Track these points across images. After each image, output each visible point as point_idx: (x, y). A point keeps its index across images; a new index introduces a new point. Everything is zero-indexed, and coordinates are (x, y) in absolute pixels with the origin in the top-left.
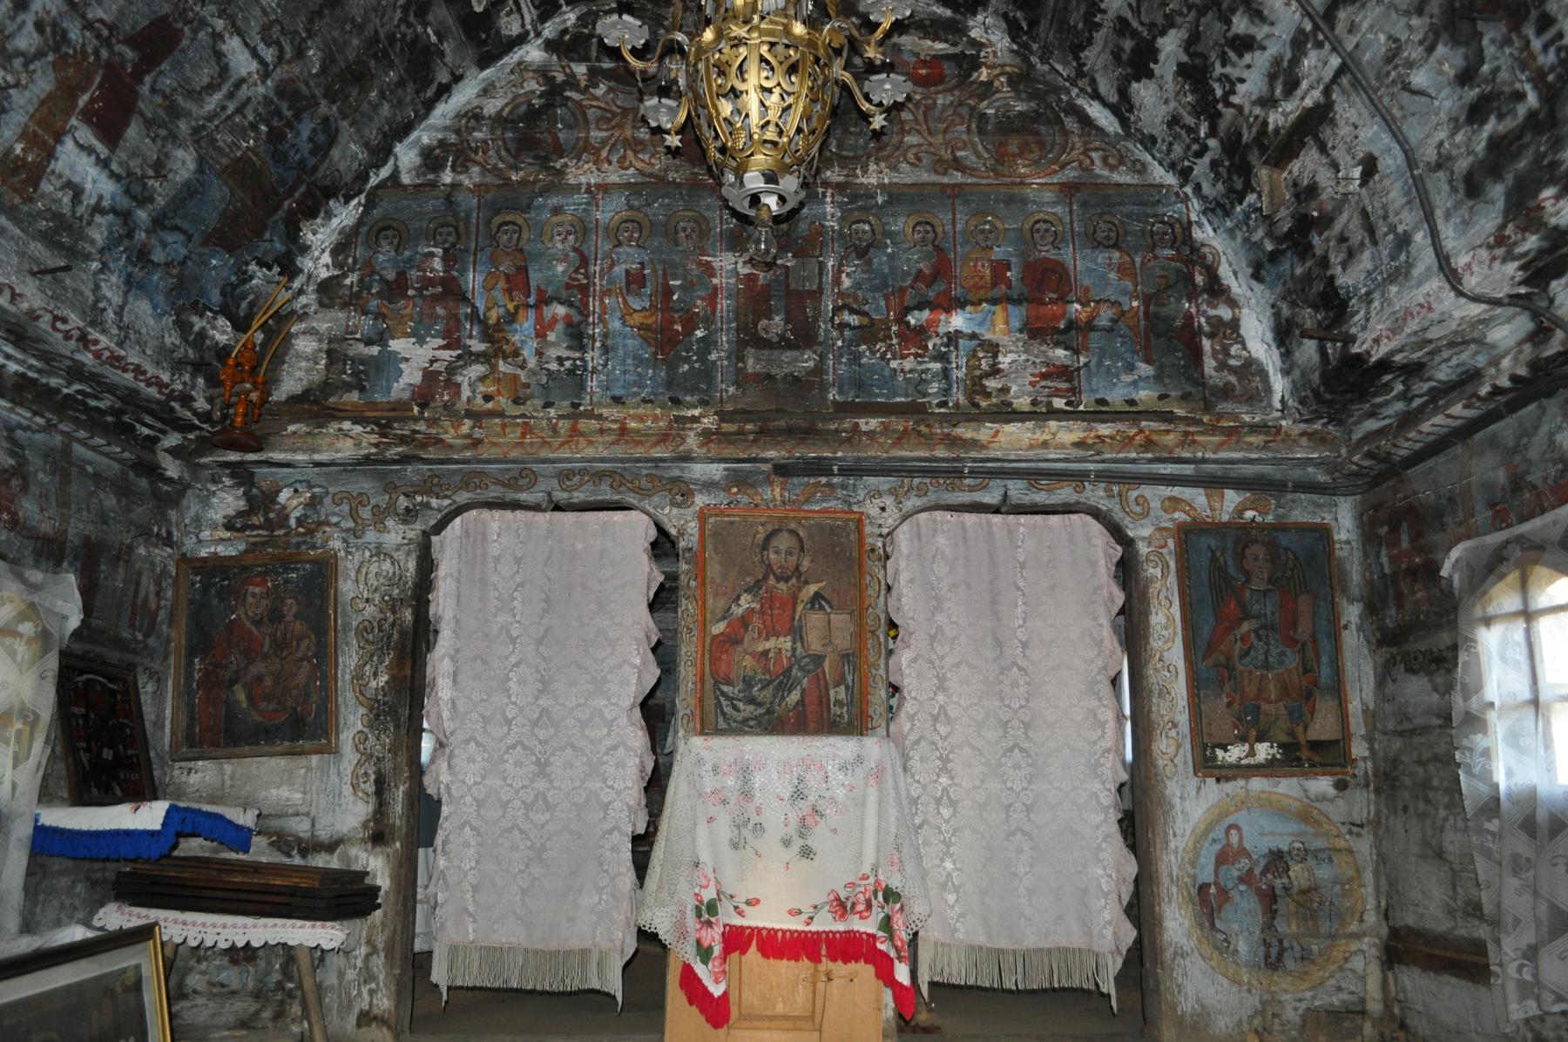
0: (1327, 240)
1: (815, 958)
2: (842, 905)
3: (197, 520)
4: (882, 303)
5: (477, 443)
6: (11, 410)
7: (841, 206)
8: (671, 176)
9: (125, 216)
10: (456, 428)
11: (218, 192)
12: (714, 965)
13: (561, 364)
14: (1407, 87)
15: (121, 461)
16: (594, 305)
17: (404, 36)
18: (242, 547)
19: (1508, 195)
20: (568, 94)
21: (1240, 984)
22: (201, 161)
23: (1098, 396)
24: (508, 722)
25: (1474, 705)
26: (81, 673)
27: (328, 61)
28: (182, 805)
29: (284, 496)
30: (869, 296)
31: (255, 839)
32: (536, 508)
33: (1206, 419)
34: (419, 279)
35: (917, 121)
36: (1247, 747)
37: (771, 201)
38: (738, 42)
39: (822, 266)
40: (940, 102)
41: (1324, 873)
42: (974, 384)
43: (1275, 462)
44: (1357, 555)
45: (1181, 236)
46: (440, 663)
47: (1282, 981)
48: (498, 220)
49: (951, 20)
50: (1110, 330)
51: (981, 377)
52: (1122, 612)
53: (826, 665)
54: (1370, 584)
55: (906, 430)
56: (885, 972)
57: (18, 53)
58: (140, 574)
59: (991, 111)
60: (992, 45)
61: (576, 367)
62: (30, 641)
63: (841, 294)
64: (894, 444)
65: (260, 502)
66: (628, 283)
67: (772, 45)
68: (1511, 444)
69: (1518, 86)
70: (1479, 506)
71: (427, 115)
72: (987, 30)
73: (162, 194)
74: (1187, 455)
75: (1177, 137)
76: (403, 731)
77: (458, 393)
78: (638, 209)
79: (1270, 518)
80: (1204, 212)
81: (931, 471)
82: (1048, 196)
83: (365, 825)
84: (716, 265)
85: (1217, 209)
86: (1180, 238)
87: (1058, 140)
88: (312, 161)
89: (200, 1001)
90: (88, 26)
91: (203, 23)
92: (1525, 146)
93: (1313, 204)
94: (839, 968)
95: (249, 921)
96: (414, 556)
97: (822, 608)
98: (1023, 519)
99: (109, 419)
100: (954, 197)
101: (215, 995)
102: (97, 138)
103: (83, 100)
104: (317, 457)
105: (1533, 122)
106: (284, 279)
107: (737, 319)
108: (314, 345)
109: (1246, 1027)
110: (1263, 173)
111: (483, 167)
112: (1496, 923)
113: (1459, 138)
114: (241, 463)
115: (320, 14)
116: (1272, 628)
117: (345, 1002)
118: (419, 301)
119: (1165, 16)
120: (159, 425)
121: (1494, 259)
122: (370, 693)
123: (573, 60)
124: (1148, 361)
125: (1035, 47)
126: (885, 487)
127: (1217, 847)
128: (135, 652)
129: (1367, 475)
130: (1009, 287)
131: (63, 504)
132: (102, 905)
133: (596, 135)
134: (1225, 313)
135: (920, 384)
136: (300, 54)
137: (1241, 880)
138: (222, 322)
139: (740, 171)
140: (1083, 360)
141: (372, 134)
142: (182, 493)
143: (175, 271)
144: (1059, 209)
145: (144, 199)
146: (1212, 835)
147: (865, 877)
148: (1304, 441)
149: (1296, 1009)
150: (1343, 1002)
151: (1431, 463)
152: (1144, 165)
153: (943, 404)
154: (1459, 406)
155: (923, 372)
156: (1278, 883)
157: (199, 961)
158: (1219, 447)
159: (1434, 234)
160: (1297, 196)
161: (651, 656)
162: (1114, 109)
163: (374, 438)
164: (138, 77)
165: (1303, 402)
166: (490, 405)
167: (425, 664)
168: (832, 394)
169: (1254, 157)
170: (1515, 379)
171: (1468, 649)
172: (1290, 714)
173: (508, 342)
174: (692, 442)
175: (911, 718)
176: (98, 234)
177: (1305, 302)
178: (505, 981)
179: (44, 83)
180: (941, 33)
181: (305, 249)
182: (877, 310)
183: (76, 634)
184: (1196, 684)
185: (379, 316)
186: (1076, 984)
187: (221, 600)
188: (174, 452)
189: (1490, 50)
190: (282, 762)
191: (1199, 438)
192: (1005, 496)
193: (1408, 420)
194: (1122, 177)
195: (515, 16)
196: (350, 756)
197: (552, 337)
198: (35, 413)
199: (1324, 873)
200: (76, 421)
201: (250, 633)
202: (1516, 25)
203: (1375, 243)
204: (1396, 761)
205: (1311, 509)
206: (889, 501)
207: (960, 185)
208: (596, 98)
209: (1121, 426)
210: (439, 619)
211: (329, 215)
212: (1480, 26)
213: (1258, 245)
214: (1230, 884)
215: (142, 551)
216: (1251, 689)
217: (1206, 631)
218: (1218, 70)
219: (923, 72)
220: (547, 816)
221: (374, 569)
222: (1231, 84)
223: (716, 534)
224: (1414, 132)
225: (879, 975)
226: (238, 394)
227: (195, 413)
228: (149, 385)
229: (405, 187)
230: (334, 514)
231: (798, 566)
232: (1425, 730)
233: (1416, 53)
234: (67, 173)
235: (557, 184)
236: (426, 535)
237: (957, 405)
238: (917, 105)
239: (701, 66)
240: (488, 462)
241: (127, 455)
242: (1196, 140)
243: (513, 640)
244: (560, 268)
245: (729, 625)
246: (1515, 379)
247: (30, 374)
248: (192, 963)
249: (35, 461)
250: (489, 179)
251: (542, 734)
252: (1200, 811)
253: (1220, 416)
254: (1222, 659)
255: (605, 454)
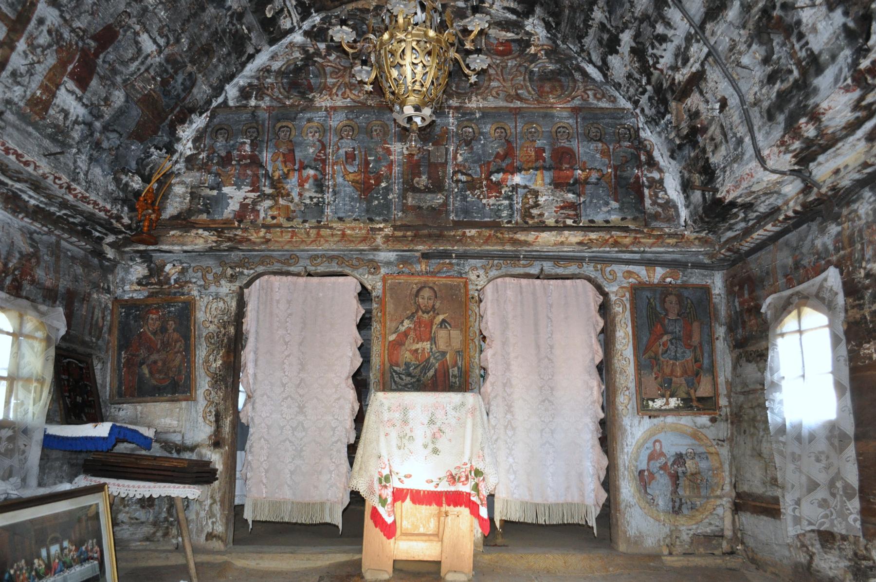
0: (705, 139)
1: (439, 504)
2: (453, 477)
3: (123, 280)
4: (478, 169)
5: (268, 241)
6: (31, 224)
7: (457, 118)
8: (369, 102)
9: (89, 125)
10: (257, 233)
11: (136, 112)
12: (388, 507)
13: (312, 200)
14: (739, 64)
15: (85, 250)
16: (329, 170)
17: (231, 30)
18: (146, 294)
19: (786, 120)
20: (315, 59)
21: (659, 521)
22: (127, 97)
23: (590, 218)
24: (284, 385)
25: (776, 377)
26: (65, 358)
27: (192, 43)
28: (118, 424)
29: (168, 268)
30: (472, 165)
31: (154, 444)
32: (298, 275)
33: (645, 230)
34: (239, 156)
35: (497, 74)
36: (665, 400)
37: (418, 120)
38: (400, 41)
39: (447, 150)
40: (509, 64)
41: (703, 465)
42: (526, 212)
43: (681, 253)
44: (724, 301)
45: (634, 135)
46: (248, 355)
47: (681, 520)
48: (279, 125)
49: (516, 21)
50: (596, 184)
51: (529, 208)
52: (603, 331)
53: (448, 356)
54: (730, 316)
55: (490, 235)
56: (474, 509)
57: (39, 46)
58: (94, 308)
59: (536, 69)
60: (537, 34)
61: (319, 202)
62: (41, 340)
63: (457, 165)
64: (484, 242)
65: (155, 271)
66: (347, 158)
67: (418, 42)
68: (795, 245)
69: (789, 66)
70: (780, 276)
71: (242, 70)
72: (535, 26)
73: (108, 113)
74: (636, 249)
75: (631, 84)
76: (229, 389)
77: (258, 215)
78: (352, 120)
79: (679, 282)
80: (646, 123)
81: (503, 257)
82: (565, 114)
83: (210, 438)
84: (392, 149)
85: (653, 121)
86: (633, 136)
87: (571, 84)
88: (183, 95)
89: (125, 527)
90: (73, 30)
91: (130, 27)
92: (793, 97)
93: (698, 121)
94: (452, 509)
95: (152, 484)
96: (235, 299)
97: (446, 327)
98: (552, 282)
99: (79, 228)
100: (516, 114)
101: (133, 524)
102: (76, 86)
103: (70, 67)
104: (185, 248)
105: (796, 85)
106: (168, 156)
107: (403, 177)
108: (184, 190)
109: (662, 543)
110: (673, 104)
111: (271, 97)
112: (783, 488)
113: (764, 91)
114: (145, 251)
115: (188, 21)
116: (678, 339)
117: (200, 528)
118: (238, 167)
119: (624, 23)
120: (104, 231)
121: (780, 152)
122: (212, 370)
123: (318, 41)
124: (616, 200)
125: (559, 36)
126: (479, 265)
127: (649, 451)
128: (91, 348)
129: (729, 260)
130: (544, 161)
131: (57, 271)
132: (76, 476)
133: (330, 81)
134: (656, 175)
135: (497, 211)
136: (178, 41)
137: (661, 468)
138: (137, 178)
139: (402, 104)
140: (582, 199)
141: (214, 80)
142: (115, 266)
143: (114, 153)
144: (571, 121)
145: (98, 117)
146: (646, 445)
147: (465, 464)
148: (697, 242)
149: (688, 534)
150: (712, 530)
151: (758, 254)
152: (615, 98)
153: (509, 222)
154: (770, 225)
155: (500, 205)
156: (680, 470)
157: (124, 507)
158: (651, 246)
159: (753, 138)
160: (690, 116)
161: (358, 352)
162: (600, 69)
163: (214, 238)
164: (96, 55)
165: (695, 222)
166: (275, 221)
167: (240, 355)
168: (452, 217)
169: (669, 96)
170: (795, 212)
171: (773, 349)
172: (688, 383)
173: (284, 189)
174: (379, 240)
175: (492, 384)
176: (76, 135)
177: (696, 170)
178: (282, 518)
179: (51, 60)
180: (511, 28)
181: (179, 140)
182: (476, 173)
183: (63, 338)
184: (639, 367)
185: (217, 175)
186: (576, 521)
187: (136, 321)
188: (111, 245)
189: (777, 48)
190: (167, 405)
191: (642, 240)
192: (542, 270)
193: (747, 232)
194: (604, 104)
195: (288, 19)
196: (202, 403)
197: (307, 186)
198: (43, 225)
199: (703, 465)
200: (63, 229)
201: (150, 339)
202: (788, 37)
203: (727, 142)
204: (741, 407)
205: (701, 277)
206: (481, 272)
207: (520, 108)
208: (330, 61)
209: (602, 234)
210: (248, 332)
211: (191, 122)
212: (772, 36)
213: (671, 141)
214: (655, 470)
215: (95, 296)
216: (667, 371)
217: (645, 340)
218: (650, 51)
219: (501, 48)
220: (304, 434)
221: (214, 306)
222: (657, 58)
223: (391, 289)
224: (744, 88)
225: (472, 513)
226: (145, 215)
227: (123, 225)
228: (100, 211)
229: (231, 108)
230: (194, 277)
231: (434, 306)
232: (754, 391)
233: (743, 47)
234: (62, 104)
235: (310, 106)
236: (241, 288)
237: (517, 223)
238: (497, 66)
239: (382, 52)
240: (273, 251)
241: (88, 246)
242: (641, 86)
243: (286, 343)
244: (311, 150)
245: (398, 336)
246: (795, 212)
247: (42, 206)
248: (121, 507)
249: (43, 250)
250: (275, 104)
251: (301, 392)
252: (640, 433)
253: (653, 229)
254: (653, 354)
255: (334, 247)
